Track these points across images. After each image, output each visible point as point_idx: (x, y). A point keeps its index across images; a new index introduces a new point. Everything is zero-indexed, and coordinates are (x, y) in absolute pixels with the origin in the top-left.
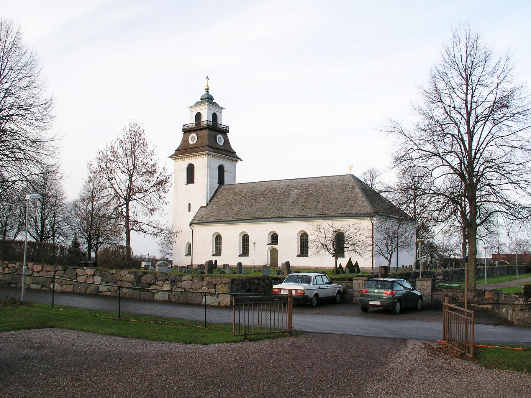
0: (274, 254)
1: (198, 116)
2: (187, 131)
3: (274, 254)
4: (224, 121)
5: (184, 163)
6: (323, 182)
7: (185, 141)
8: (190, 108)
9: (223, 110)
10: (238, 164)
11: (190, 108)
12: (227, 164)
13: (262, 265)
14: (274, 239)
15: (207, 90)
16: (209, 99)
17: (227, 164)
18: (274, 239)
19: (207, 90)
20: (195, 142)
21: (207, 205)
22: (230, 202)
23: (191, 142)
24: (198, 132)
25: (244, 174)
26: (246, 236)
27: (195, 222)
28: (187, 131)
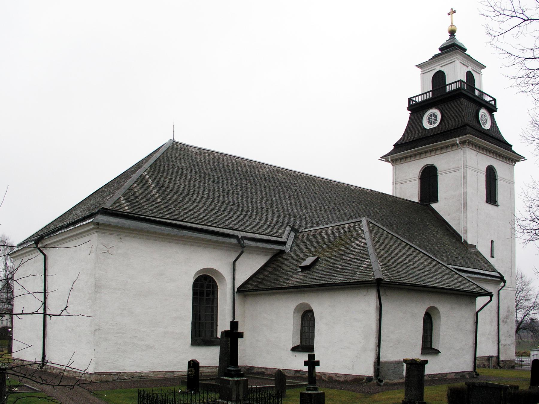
2: (417, 109)
4: (487, 85)
8: (419, 66)
9: (483, 71)
11: (419, 66)
12: (500, 167)
15: (452, 33)
16: (452, 48)
17: (500, 167)
19: (452, 33)
20: (436, 125)
23: (427, 125)
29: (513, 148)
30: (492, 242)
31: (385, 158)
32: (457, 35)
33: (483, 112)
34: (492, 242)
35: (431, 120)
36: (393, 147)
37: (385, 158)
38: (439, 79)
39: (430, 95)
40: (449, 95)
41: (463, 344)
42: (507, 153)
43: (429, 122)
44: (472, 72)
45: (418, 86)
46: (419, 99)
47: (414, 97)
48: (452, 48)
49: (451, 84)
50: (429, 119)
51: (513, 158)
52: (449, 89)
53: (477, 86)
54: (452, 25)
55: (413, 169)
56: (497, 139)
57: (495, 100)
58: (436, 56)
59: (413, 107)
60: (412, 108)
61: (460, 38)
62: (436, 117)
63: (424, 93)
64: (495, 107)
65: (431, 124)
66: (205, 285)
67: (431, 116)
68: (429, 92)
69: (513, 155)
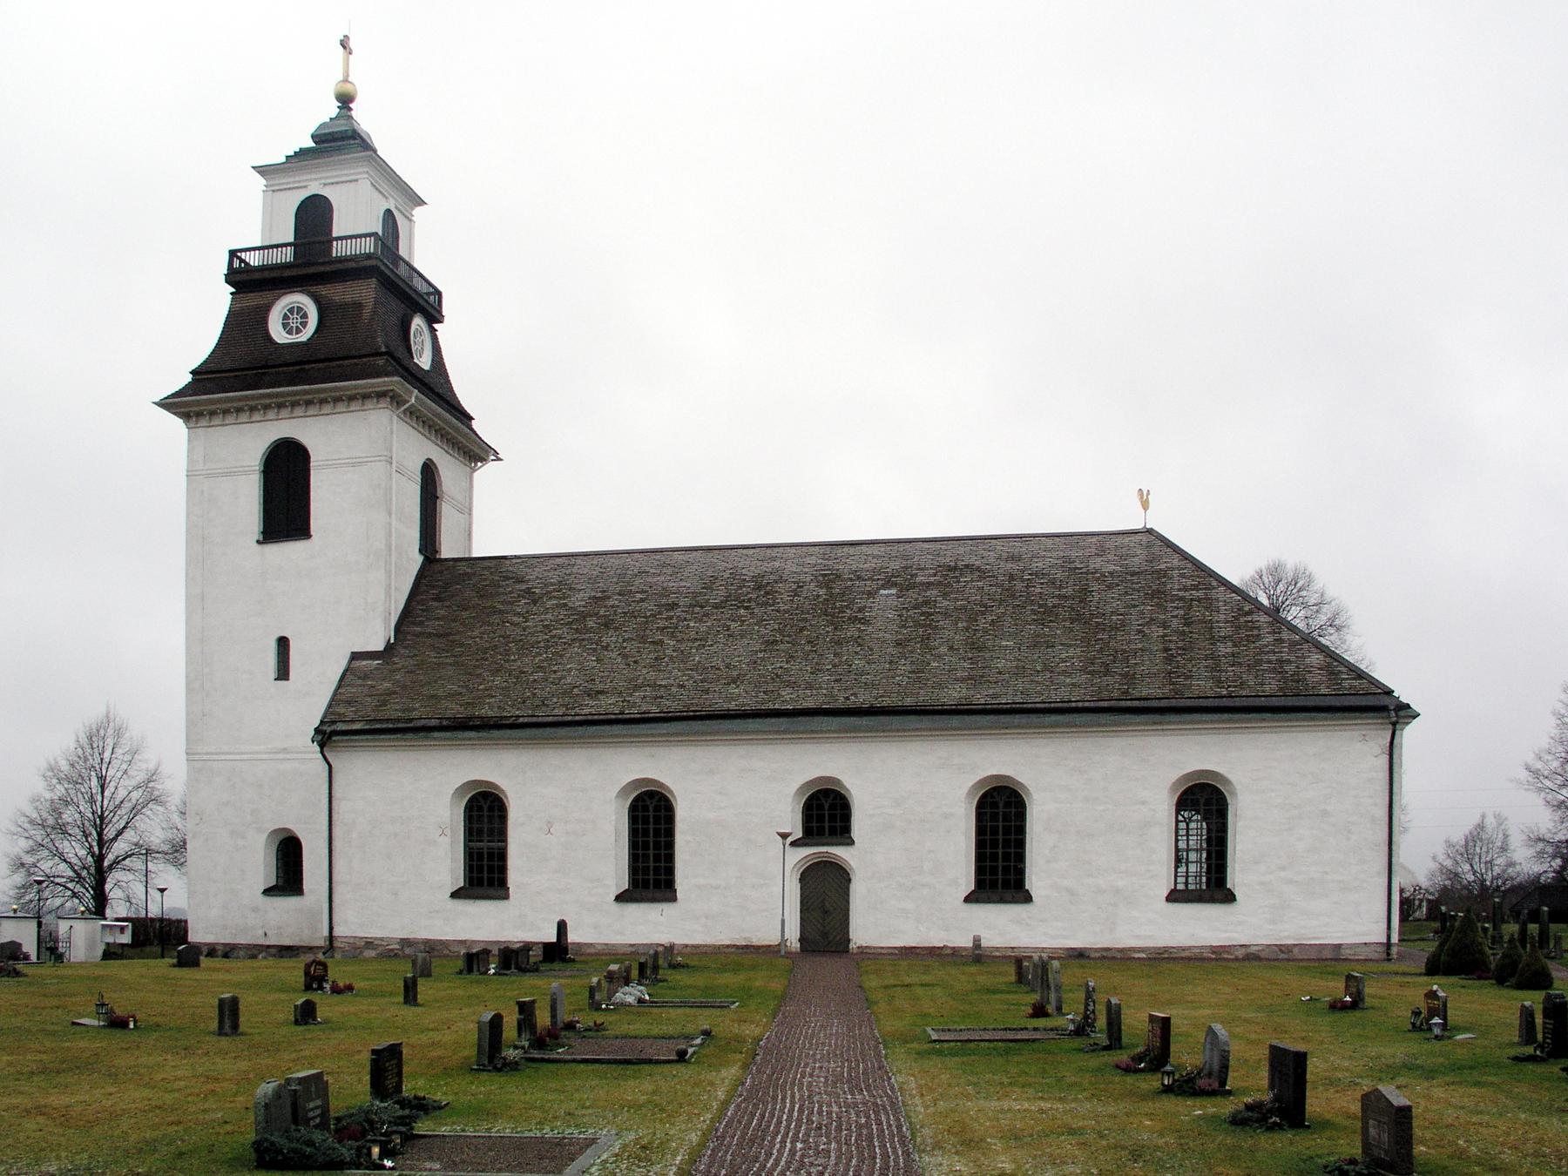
0: (825, 893)
1: (314, 215)
2: (250, 282)
3: (825, 893)
5: (248, 442)
6: (1013, 558)
7: (243, 326)
8: (262, 170)
10: (485, 475)
11: (262, 170)
13: (851, 936)
14: (826, 813)
15: (345, 100)
16: (340, 141)
17: (449, 470)
18: (826, 813)
19: (345, 100)
20: (304, 336)
21: (389, 647)
22: (477, 655)
23: (278, 334)
24: (324, 290)
25: (504, 518)
26: (651, 805)
27: (341, 727)
28: (250, 282)
29: (475, 424)
30: (283, 643)
31: (168, 404)
33: (418, 322)
34: (283, 643)
35: (292, 320)
36: (189, 378)
37: (168, 404)
38: (314, 217)
39: (287, 255)
40: (340, 266)
41: (1321, 860)
42: (457, 429)
43: (285, 326)
44: (396, 213)
45: (257, 224)
46: (254, 259)
47: (246, 250)
48: (340, 141)
49: (346, 238)
50: (286, 317)
51: (475, 452)
52: (339, 250)
53: (402, 252)
54: (346, 80)
55: (248, 442)
56: (447, 402)
57: (439, 294)
58: (302, 154)
59: (245, 277)
60: (238, 278)
61: (364, 117)
62: (305, 316)
63: (272, 247)
64: (440, 312)
65: (289, 332)
66: (1001, 805)
67: (291, 310)
68: (285, 245)
69: (465, 436)
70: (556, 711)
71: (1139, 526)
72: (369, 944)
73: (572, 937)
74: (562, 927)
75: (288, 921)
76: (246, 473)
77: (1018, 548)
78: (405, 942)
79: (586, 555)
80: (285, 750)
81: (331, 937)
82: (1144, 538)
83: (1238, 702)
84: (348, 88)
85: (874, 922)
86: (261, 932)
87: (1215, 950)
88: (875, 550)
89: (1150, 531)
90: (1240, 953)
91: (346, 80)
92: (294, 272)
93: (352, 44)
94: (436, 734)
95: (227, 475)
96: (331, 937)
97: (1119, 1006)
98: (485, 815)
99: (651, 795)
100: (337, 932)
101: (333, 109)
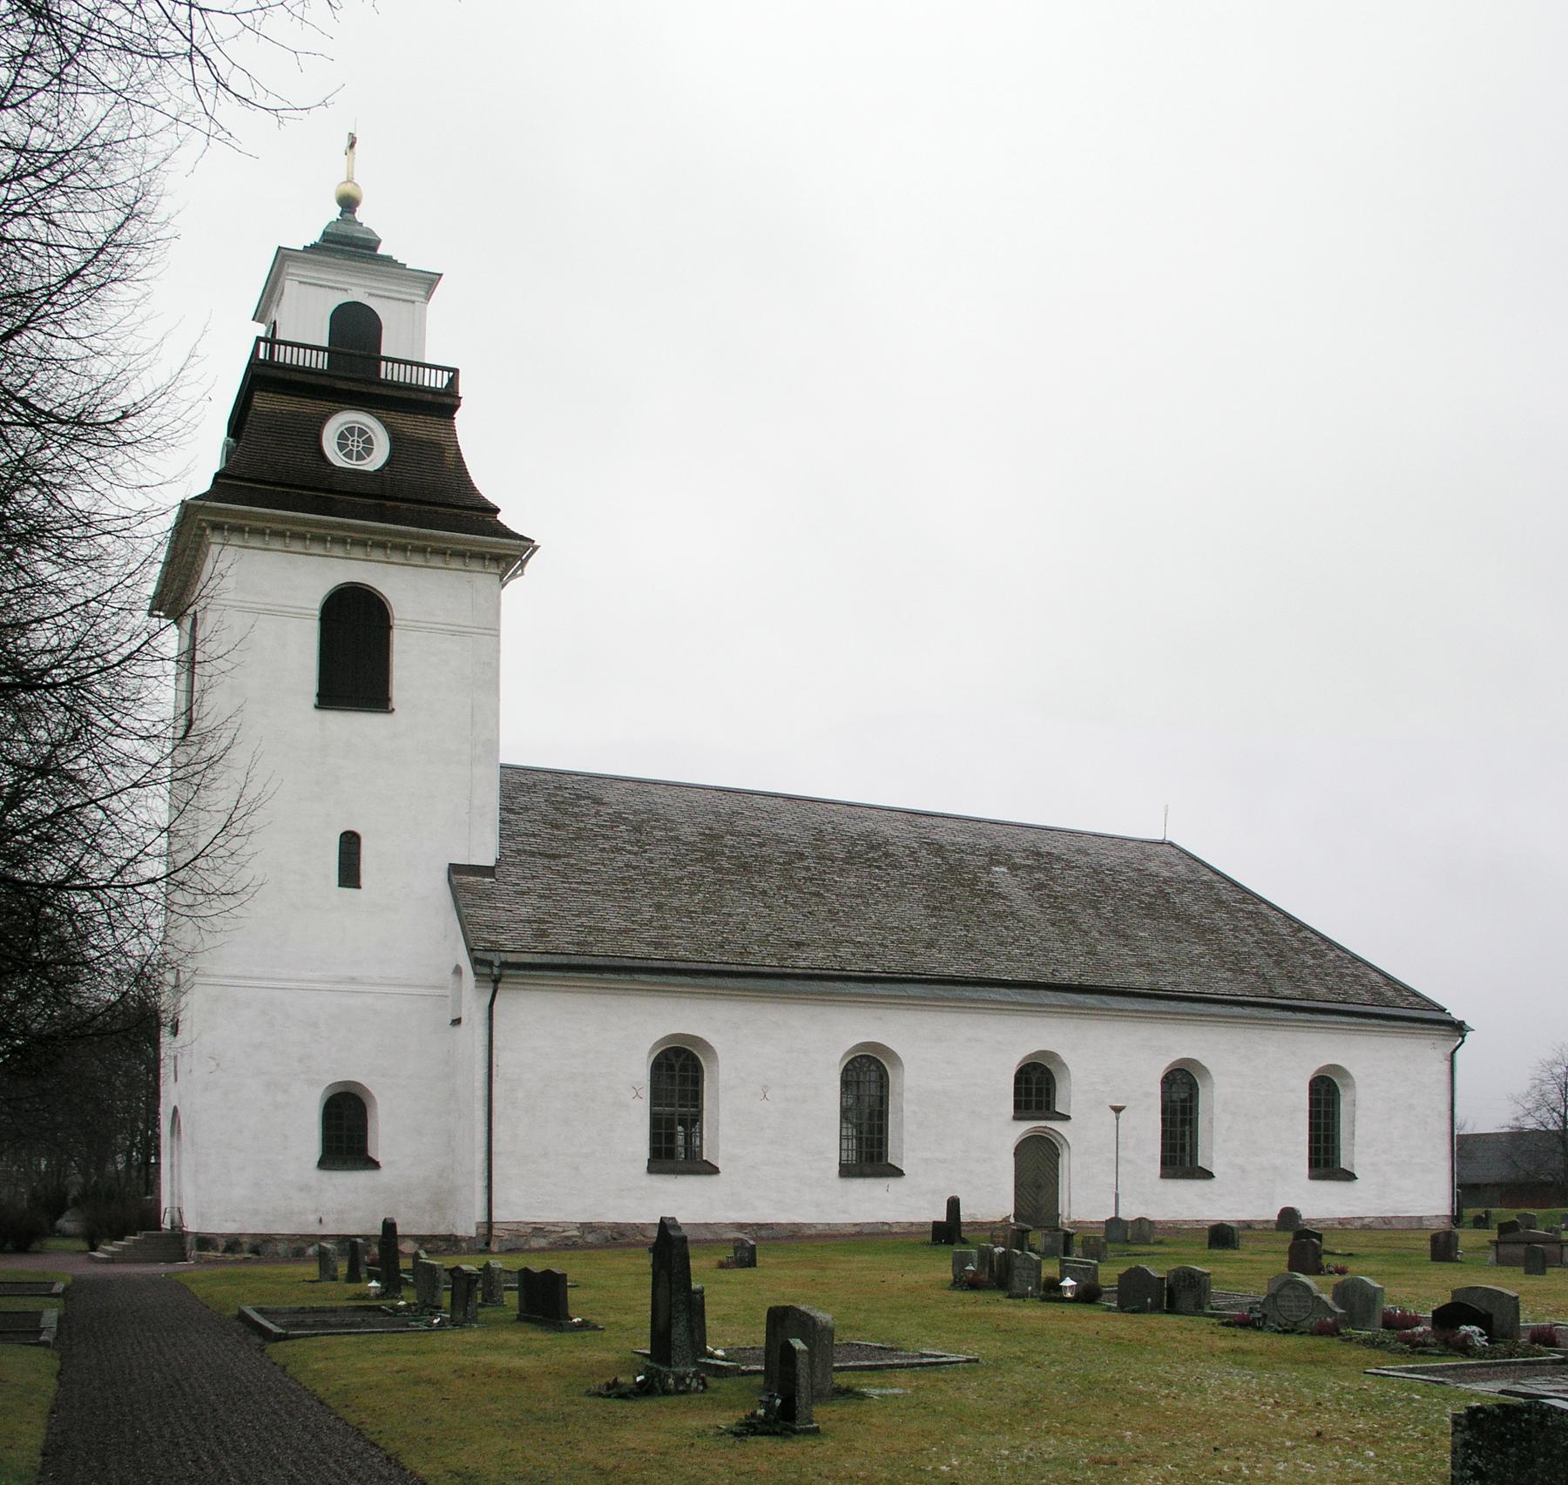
0: (1038, 1165)
3: (1038, 1165)
14: (1036, 1087)
15: (348, 204)
16: (347, 244)
19: (348, 204)
24: (398, 419)
32: (361, 215)
39: (321, 361)
48: (347, 244)
54: (350, 181)
65: (349, 455)
68: (318, 349)
70: (767, 961)
71: (1160, 837)
72: (539, 1230)
73: (965, 1215)
74: (953, 1205)
75: (348, 1204)
76: (297, 616)
77: (692, 795)
78: (587, 1227)
79: (668, 784)
80: (353, 980)
81: (490, 1223)
82: (1167, 848)
83: (588, 960)
84: (348, 188)
85: (1084, 1199)
86: (313, 1218)
87: (1341, 1221)
88: (950, 824)
89: (1171, 844)
90: (1358, 1224)
91: (350, 181)
92: (323, 381)
93: (346, 143)
94: (643, 977)
95: (269, 612)
96: (490, 1223)
97: (701, 1292)
98: (678, 1076)
99: (678, 1051)
100: (497, 1216)
101: (335, 212)
